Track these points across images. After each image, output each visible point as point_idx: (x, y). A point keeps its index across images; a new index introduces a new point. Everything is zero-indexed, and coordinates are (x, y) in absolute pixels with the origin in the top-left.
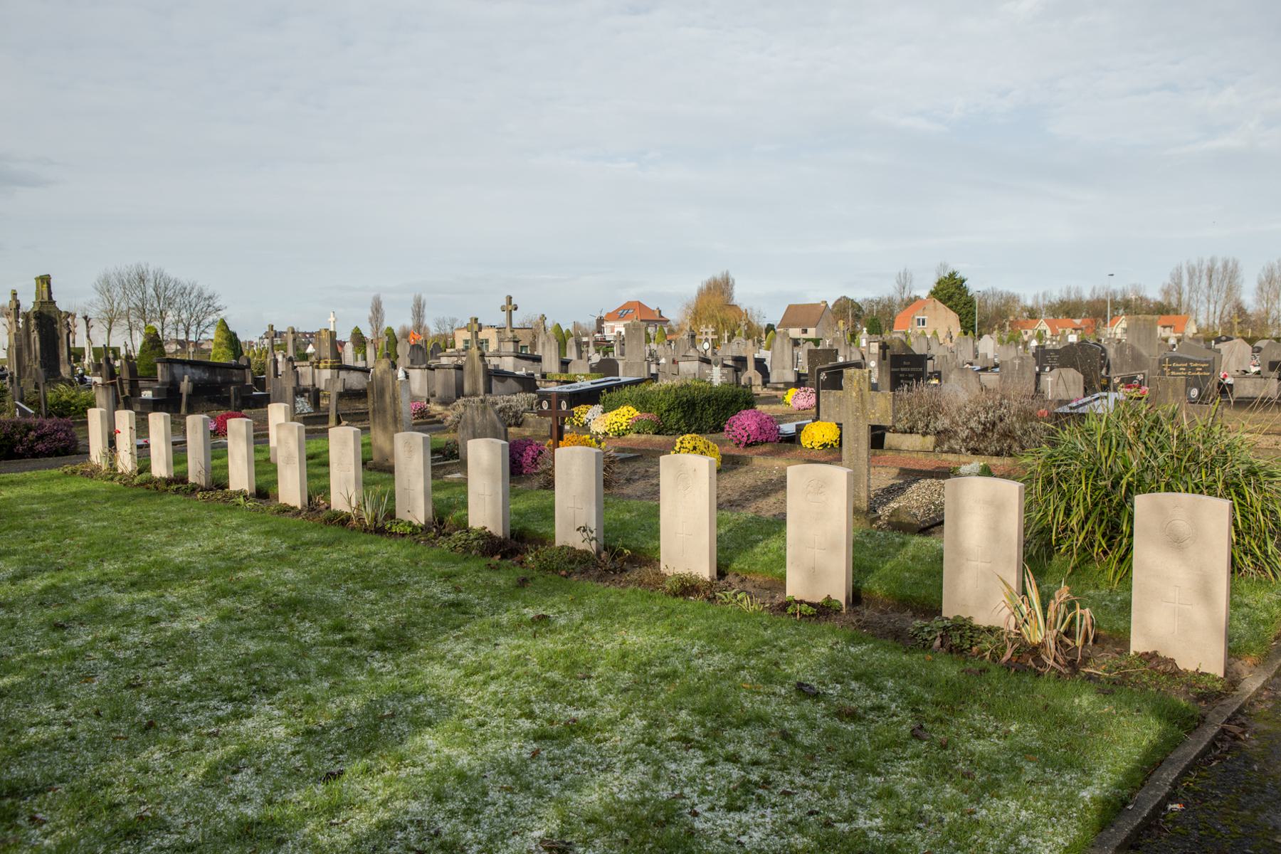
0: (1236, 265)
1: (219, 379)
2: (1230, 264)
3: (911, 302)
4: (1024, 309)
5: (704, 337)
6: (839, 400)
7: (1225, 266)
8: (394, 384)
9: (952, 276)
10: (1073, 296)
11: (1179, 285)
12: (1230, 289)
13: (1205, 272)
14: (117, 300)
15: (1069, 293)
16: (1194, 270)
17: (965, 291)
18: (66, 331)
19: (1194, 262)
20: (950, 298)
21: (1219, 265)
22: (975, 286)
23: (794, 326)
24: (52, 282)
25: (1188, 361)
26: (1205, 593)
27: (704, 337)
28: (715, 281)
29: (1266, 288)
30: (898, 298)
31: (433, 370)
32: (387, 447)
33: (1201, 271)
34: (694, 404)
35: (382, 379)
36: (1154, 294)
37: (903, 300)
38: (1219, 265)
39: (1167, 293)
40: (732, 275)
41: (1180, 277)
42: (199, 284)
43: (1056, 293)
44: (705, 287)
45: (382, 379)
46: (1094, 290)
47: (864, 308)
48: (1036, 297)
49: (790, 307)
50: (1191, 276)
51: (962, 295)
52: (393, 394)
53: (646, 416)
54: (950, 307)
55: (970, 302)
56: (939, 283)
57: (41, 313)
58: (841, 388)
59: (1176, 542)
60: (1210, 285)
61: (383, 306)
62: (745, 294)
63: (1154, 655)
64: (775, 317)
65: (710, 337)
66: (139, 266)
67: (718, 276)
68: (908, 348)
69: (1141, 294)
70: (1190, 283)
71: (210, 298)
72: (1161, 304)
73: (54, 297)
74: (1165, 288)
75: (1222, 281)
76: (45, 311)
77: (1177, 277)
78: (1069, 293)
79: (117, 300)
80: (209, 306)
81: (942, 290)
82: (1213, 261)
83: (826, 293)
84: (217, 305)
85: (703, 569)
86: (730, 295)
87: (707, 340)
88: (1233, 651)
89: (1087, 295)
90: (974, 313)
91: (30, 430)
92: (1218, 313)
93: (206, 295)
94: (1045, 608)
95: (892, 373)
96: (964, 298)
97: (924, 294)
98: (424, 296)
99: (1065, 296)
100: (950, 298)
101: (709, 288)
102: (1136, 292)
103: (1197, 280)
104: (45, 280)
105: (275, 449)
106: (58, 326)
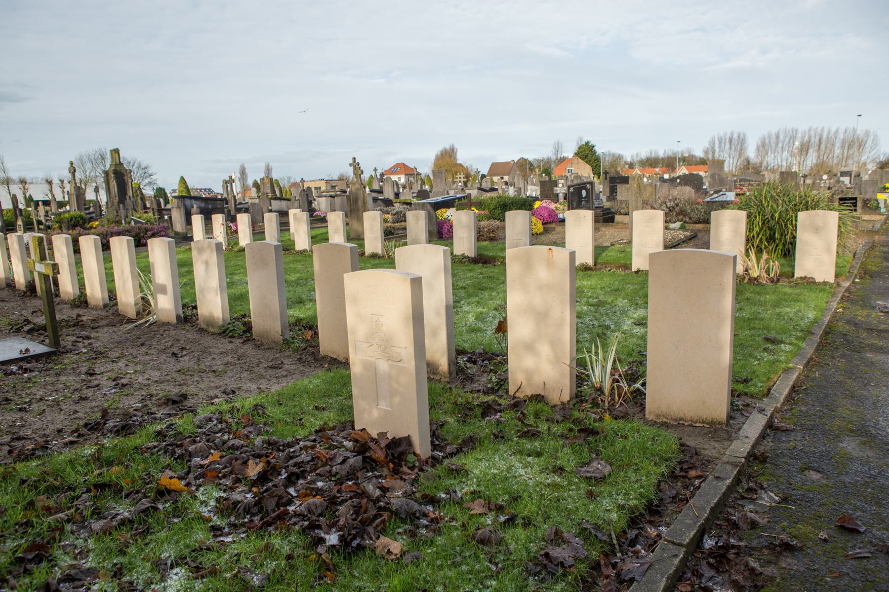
0: (745, 136)
1: (210, 207)
2: (742, 135)
3: (563, 160)
4: (626, 163)
5: (458, 180)
6: (628, 189)
7: (739, 137)
8: (364, 196)
9: (587, 143)
10: (653, 155)
11: (713, 147)
12: (741, 149)
13: (728, 140)
14: (88, 171)
15: (651, 153)
16: (721, 138)
17: (595, 152)
18: (130, 181)
19: (722, 134)
20: (586, 157)
21: (735, 136)
22: (599, 150)
23: (496, 175)
24: (120, 152)
25: (749, 181)
26: (828, 250)
27: (458, 180)
28: (446, 150)
29: (761, 149)
30: (554, 157)
31: (334, 197)
32: (360, 229)
33: (725, 140)
34: (506, 206)
35: (356, 194)
36: (699, 153)
37: (557, 159)
38: (735, 136)
39: (706, 152)
40: (456, 146)
41: (714, 143)
42: (138, 160)
43: (644, 155)
44: (439, 154)
45: (356, 194)
46: (665, 151)
47: (534, 164)
48: (632, 156)
49: (493, 164)
50: (720, 143)
51: (593, 155)
52: (364, 201)
53: (482, 212)
54: (587, 162)
55: (597, 159)
56: (580, 148)
57: (116, 170)
58: (628, 183)
59: (817, 230)
60: (731, 148)
61: (247, 171)
62: (462, 157)
63: (805, 278)
64: (485, 171)
65: (462, 180)
66: (100, 150)
67: (448, 147)
68: (619, 173)
69: (692, 153)
70: (720, 147)
71: (146, 168)
72: (703, 159)
73: (121, 161)
74: (705, 149)
75: (737, 145)
76: (118, 169)
77: (712, 144)
78: (651, 153)
79: (88, 171)
80: (145, 173)
81: (582, 152)
82: (732, 133)
83: (510, 156)
84: (150, 172)
85: (590, 261)
86: (455, 159)
87: (460, 182)
88: (837, 276)
89: (661, 154)
90: (600, 166)
91: (147, 231)
92: (735, 164)
93: (143, 166)
94: (758, 264)
95: (610, 187)
96: (594, 157)
97: (570, 155)
98: (246, 166)
99: (649, 155)
100: (586, 157)
101: (442, 154)
102: (689, 152)
103: (723, 145)
104: (116, 151)
105: (293, 234)
106: (126, 178)
